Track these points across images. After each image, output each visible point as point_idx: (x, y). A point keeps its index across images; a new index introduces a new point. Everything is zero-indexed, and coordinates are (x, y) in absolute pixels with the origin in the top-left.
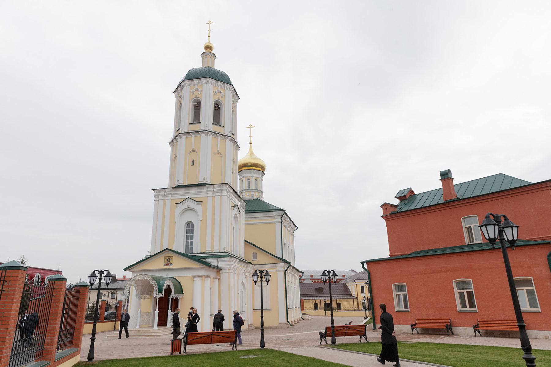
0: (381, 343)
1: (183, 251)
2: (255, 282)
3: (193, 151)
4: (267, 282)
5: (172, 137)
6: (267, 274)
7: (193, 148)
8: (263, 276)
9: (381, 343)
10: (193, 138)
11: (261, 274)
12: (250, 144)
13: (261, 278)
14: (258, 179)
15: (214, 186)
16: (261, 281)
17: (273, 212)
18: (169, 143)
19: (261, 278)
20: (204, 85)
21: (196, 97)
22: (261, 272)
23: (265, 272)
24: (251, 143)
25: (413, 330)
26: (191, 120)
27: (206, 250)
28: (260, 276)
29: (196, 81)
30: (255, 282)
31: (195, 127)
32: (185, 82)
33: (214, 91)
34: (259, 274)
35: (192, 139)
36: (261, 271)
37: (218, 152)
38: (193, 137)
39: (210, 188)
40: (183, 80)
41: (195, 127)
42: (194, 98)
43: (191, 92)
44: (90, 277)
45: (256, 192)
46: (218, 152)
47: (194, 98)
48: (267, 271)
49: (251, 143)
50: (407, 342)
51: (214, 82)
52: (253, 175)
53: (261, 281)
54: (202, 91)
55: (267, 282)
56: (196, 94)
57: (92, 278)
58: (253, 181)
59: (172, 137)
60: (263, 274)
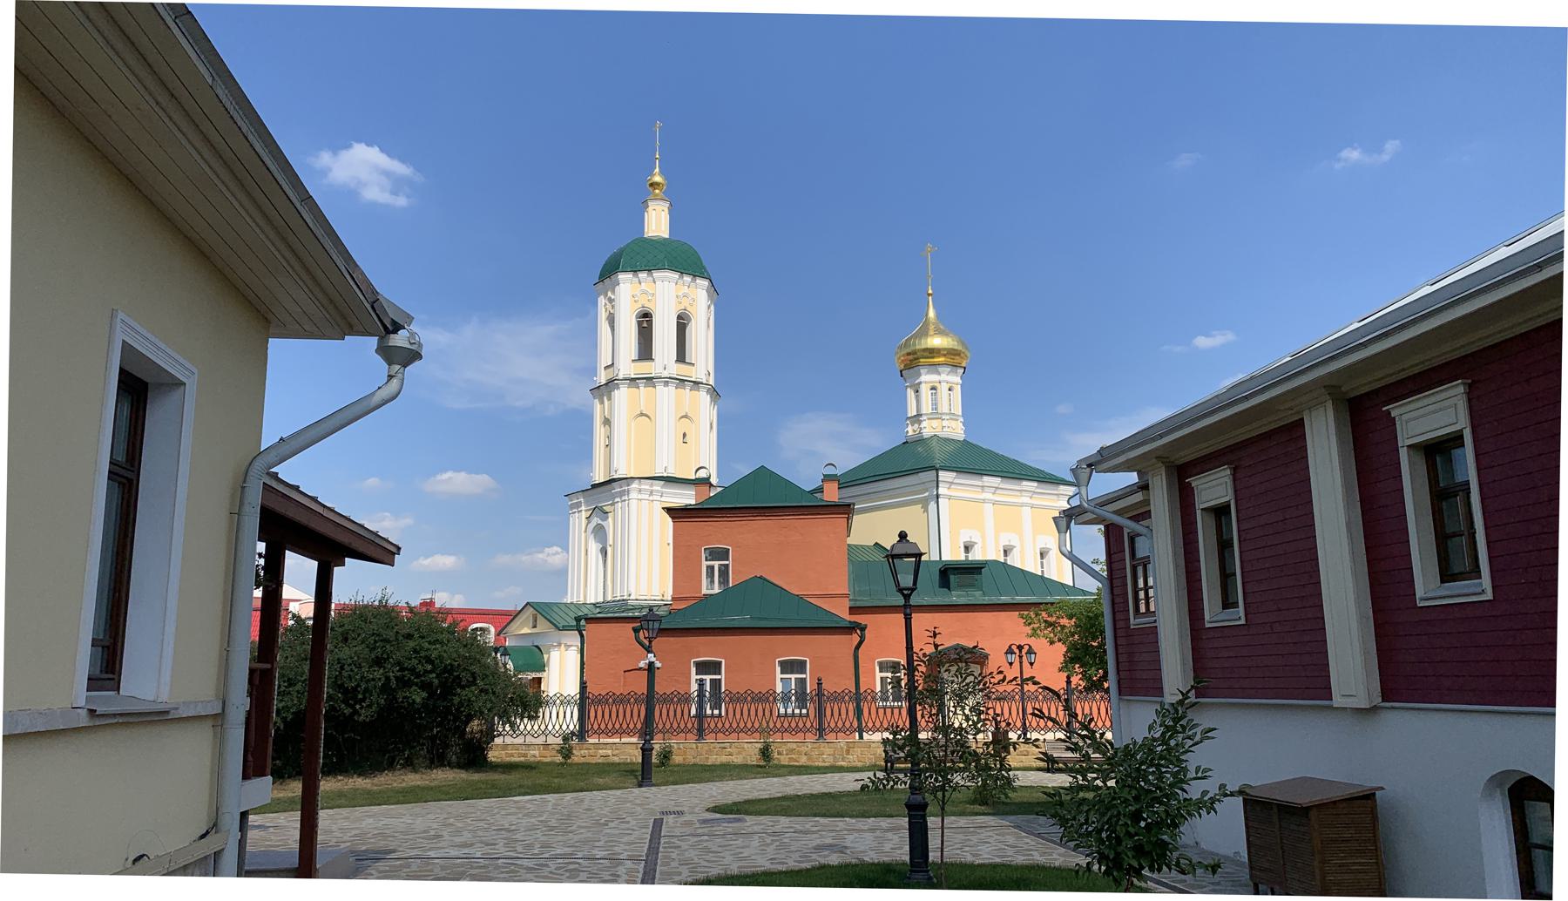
2: (1011, 664)
3: (686, 416)
4: (1031, 664)
6: (1030, 652)
8: (1025, 655)
11: (1020, 651)
13: (1021, 657)
14: (937, 385)
16: (1021, 663)
17: (920, 474)
19: (1021, 657)
22: (1020, 648)
23: (1026, 648)
25: (157, 718)
26: (634, 355)
28: (1018, 654)
30: (1011, 664)
31: (645, 368)
34: (1017, 651)
36: (1020, 645)
38: (643, 390)
41: (645, 368)
44: (1006, 653)
48: (1030, 647)
52: (943, 377)
53: (1021, 663)
55: (1031, 664)
57: (1009, 656)
60: (1024, 651)
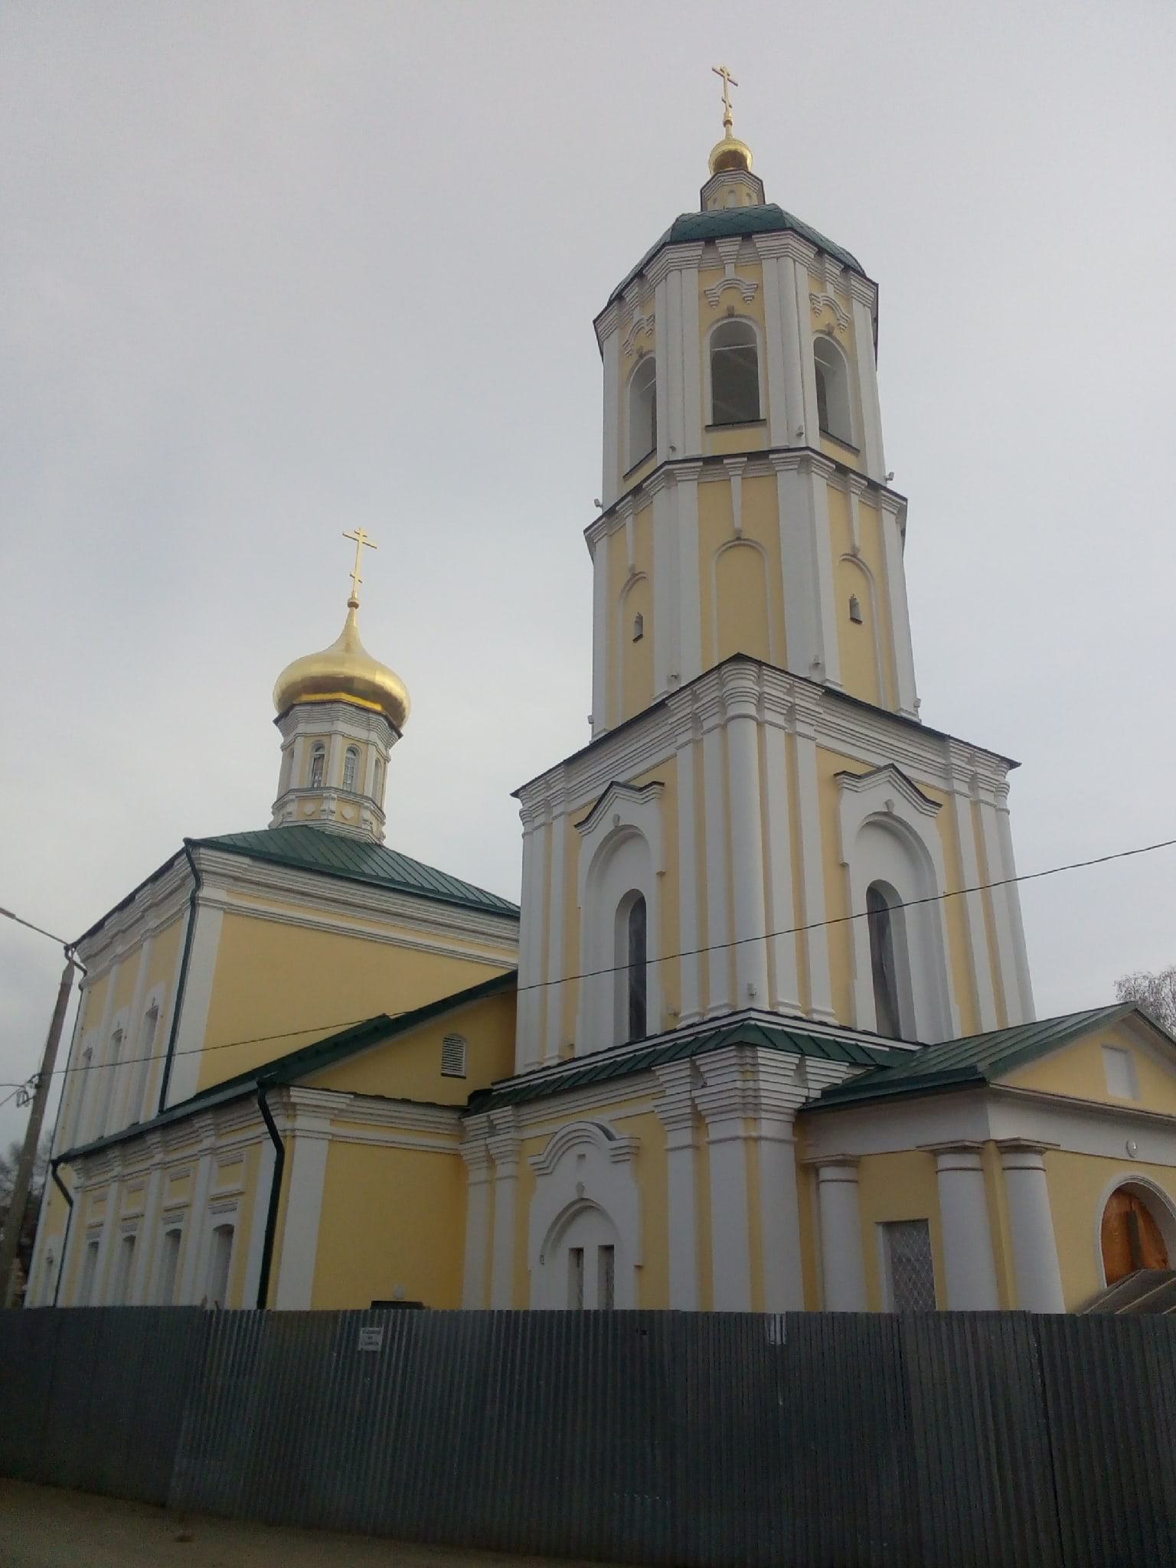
0: (54, 1305)
1: (846, 997)
5: (596, 501)
7: (738, 525)
9: (54, 1305)
10: (736, 482)
12: (348, 610)
15: (694, 693)
18: (585, 531)
20: (768, 266)
21: (731, 316)
24: (353, 605)
27: (547, 1056)
29: (728, 247)
32: (674, 254)
33: (811, 295)
35: (730, 485)
37: (739, 541)
39: (682, 709)
40: (664, 245)
42: (718, 321)
43: (704, 294)
45: (347, 801)
46: (739, 541)
47: (718, 321)
49: (353, 605)
50: (675, 1031)
51: (812, 256)
54: (758, 288)
56: (731, 299)
58: (338, 751)
59: (596, 501)
